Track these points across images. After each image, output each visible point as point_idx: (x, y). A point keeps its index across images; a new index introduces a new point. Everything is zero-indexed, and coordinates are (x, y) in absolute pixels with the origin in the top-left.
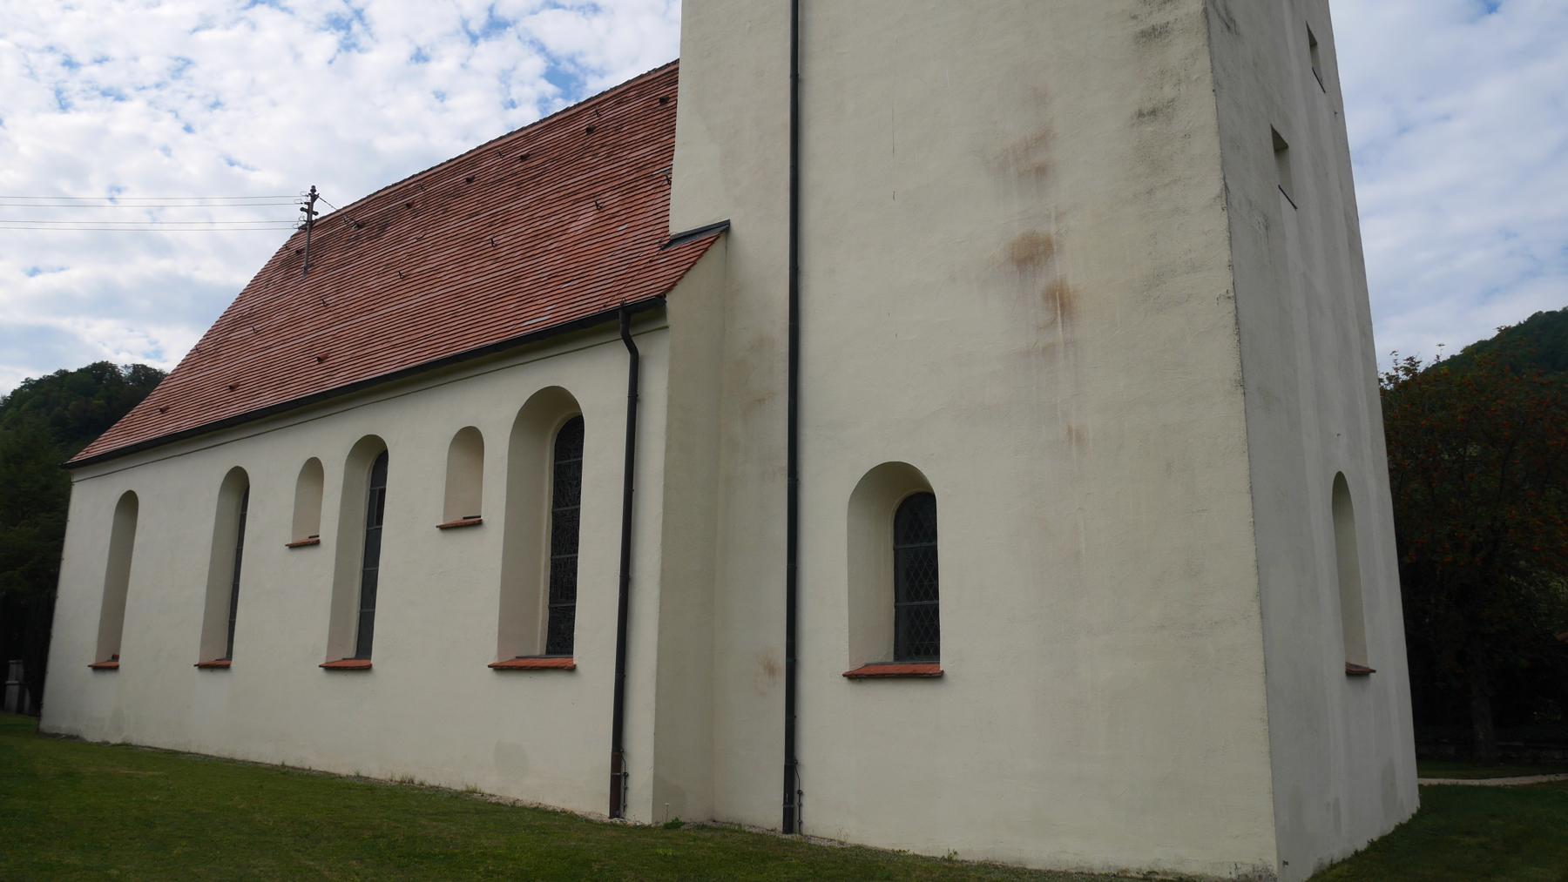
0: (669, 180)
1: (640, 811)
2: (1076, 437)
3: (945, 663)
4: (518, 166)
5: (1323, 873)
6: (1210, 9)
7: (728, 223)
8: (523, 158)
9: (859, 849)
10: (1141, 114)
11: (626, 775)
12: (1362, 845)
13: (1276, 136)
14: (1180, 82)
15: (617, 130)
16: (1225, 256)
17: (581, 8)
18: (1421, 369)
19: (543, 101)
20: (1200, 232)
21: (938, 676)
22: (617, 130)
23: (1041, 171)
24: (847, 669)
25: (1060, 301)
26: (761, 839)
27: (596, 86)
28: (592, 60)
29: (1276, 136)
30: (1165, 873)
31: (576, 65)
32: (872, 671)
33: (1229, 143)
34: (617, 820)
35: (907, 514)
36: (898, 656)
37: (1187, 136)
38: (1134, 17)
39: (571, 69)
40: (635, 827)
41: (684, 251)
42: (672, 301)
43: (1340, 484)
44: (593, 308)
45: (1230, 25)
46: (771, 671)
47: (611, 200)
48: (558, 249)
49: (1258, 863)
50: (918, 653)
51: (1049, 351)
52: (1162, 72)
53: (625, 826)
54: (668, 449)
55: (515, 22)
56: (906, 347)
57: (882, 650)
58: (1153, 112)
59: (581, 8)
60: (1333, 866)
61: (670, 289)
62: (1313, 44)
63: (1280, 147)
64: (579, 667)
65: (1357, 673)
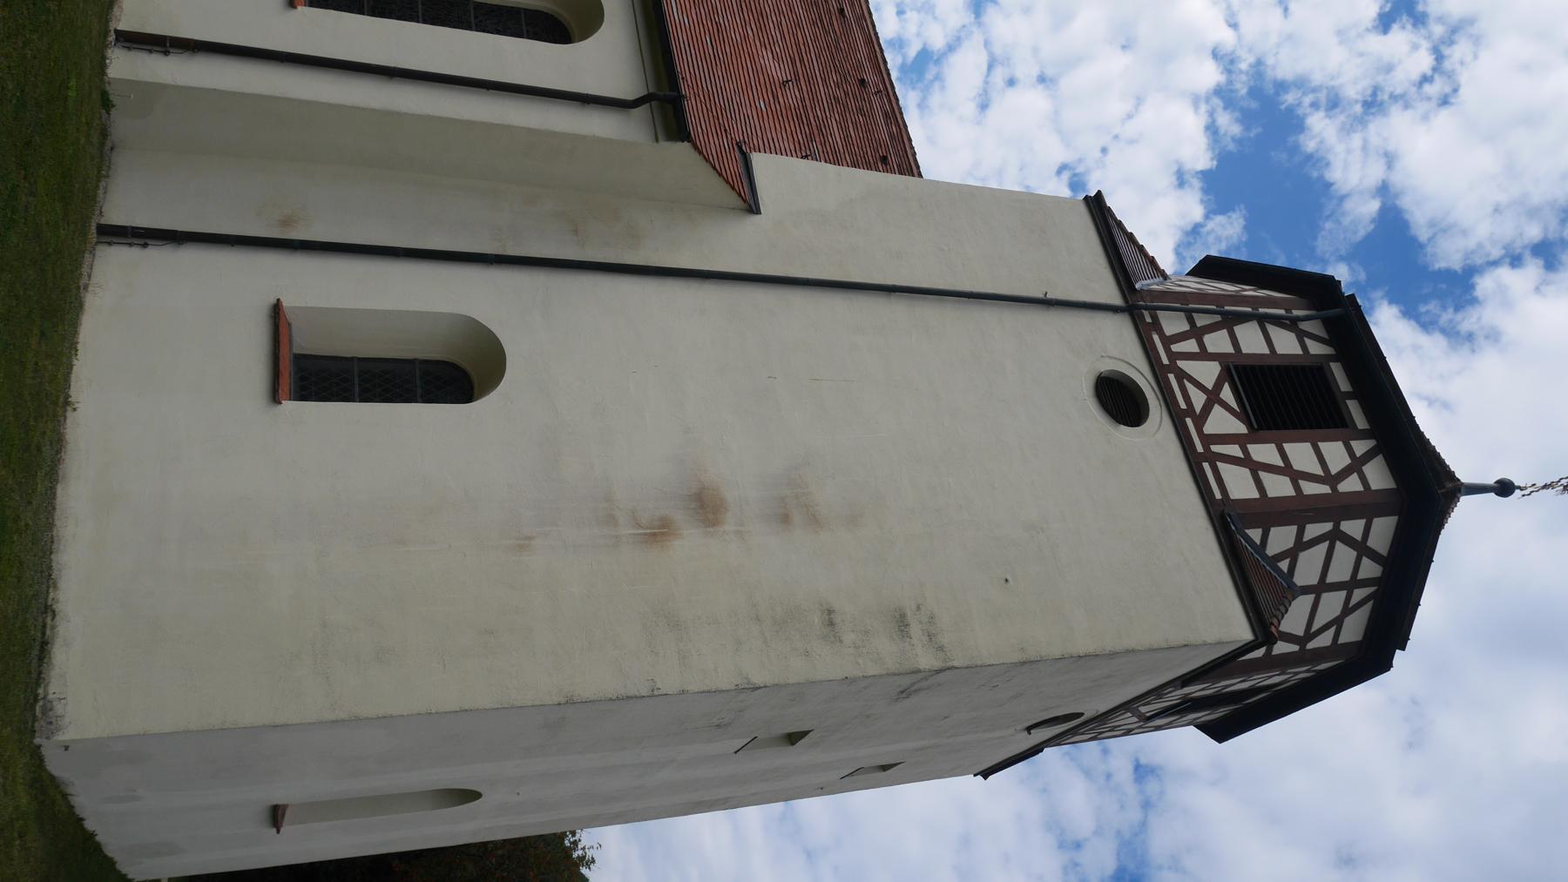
0: (806, 157)
1: (123, 65)
2: (523, 545)
3: (289, 406)
4: (834, 5)
5: (57, 787)
6: (920, 676)
7: (758, 212)
8: (841, 11)
9: (79, 307)
10: (830, 612)
11: (166, 53)
12: (89, 825)
13: (804, 734)
14: (857, 647)
15: (860, 110)
16: (693, 687)
17: (986, 92)
18: (584, 870)
19: (899, 43)
20: (716, 663)
21: (275, 398)
22: (860, 110)
23: (785, 519)
24: (285, 303)
25: (658, 533)
26: (90, 199)
27: (908, 99)
28: (935, 99)
29: (804, 734)
30: (53, 628)
31: (932, 82)
32: (282, 330)
33: (797, 692)
34: (112, 37)
35: (454, 374)
36: (300, 360)
37: (807, 654)
38: (918, 608)
39: (929, 76)
40: (104, 58)
41: (735, 166)
42: (685, 147)
43: (471, 796)
44: (683, 65)
45: (905, 693)
46: (286, 222)
47: (791, 97)
48: (746, 37)
49: (67, 720)
50: (302, 379)
51: (611, 520)
52: (867, 632)
53: (106, 46)
54: (530, 131)
55: (980, 24)
56: (611, 382)
57: (307, 341)
58: (831, 624)
59: (986, 92)
60: (65, 796)
61: (696, 147)
62: (885, 768)
63: (793, 738)
64: (293, 12)
65: (276, 816)
